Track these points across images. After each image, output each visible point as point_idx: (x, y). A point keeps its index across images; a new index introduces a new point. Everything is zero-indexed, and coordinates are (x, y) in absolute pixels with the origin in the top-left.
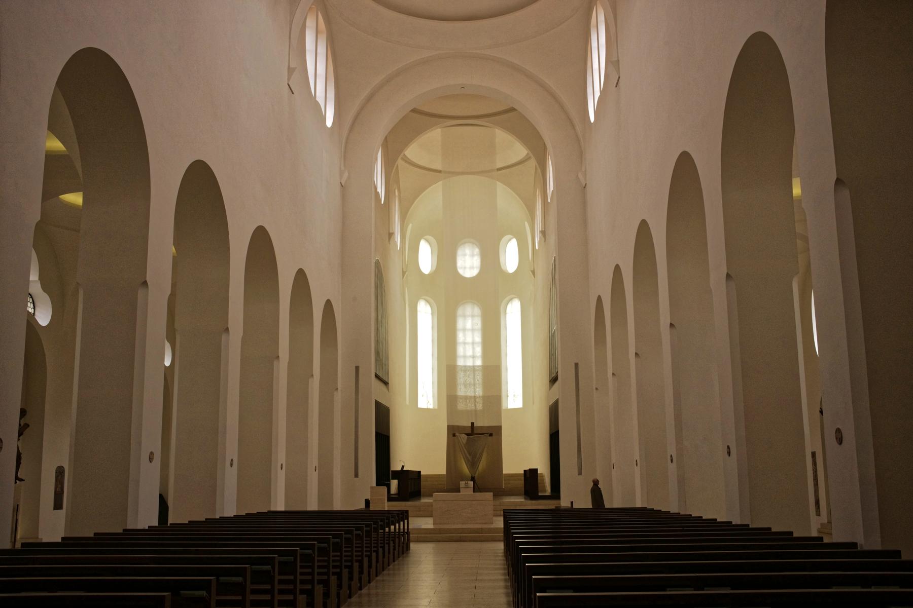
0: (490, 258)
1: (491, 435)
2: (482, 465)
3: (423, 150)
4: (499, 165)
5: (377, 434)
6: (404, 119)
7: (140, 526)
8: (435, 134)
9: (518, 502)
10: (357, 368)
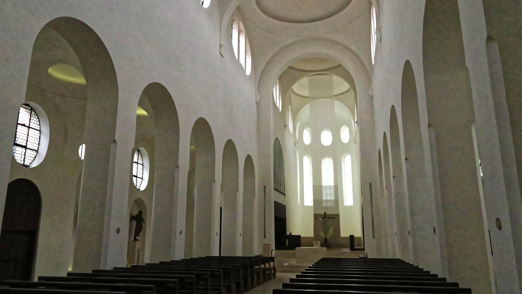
0: (336, 136)
1: (334, 218)
2: (331, 231)
3: (301, 86)
4: (336, 93)
7: (109, 267)
8: (305, 80)
9: (346, 253)
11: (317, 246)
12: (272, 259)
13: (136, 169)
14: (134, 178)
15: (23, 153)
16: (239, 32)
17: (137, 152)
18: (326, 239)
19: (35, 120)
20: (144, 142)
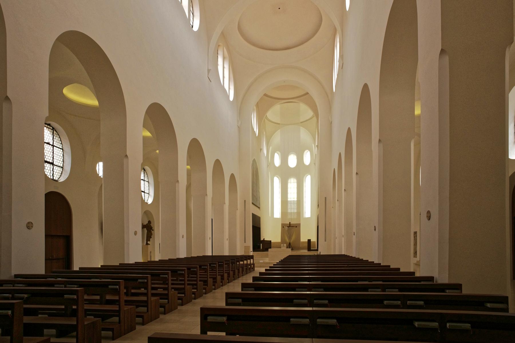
0: (300, 159)
2: (293, 238)
3: (274, 114)
4: (302, 120)
5: (253, 226)
6: (262, 99)
7: (132, 261)
8: (277, 108)
9: (305, 252)
10: (245, 201)
11: (284, 247)
12: (252, 257)
13: (144, 186)
14: (143, 193)
15: (52, 170)
16: (224, 58)
17: (143, 171)
18: (290, 243)
19: (57, 139)
20: (149, 162)
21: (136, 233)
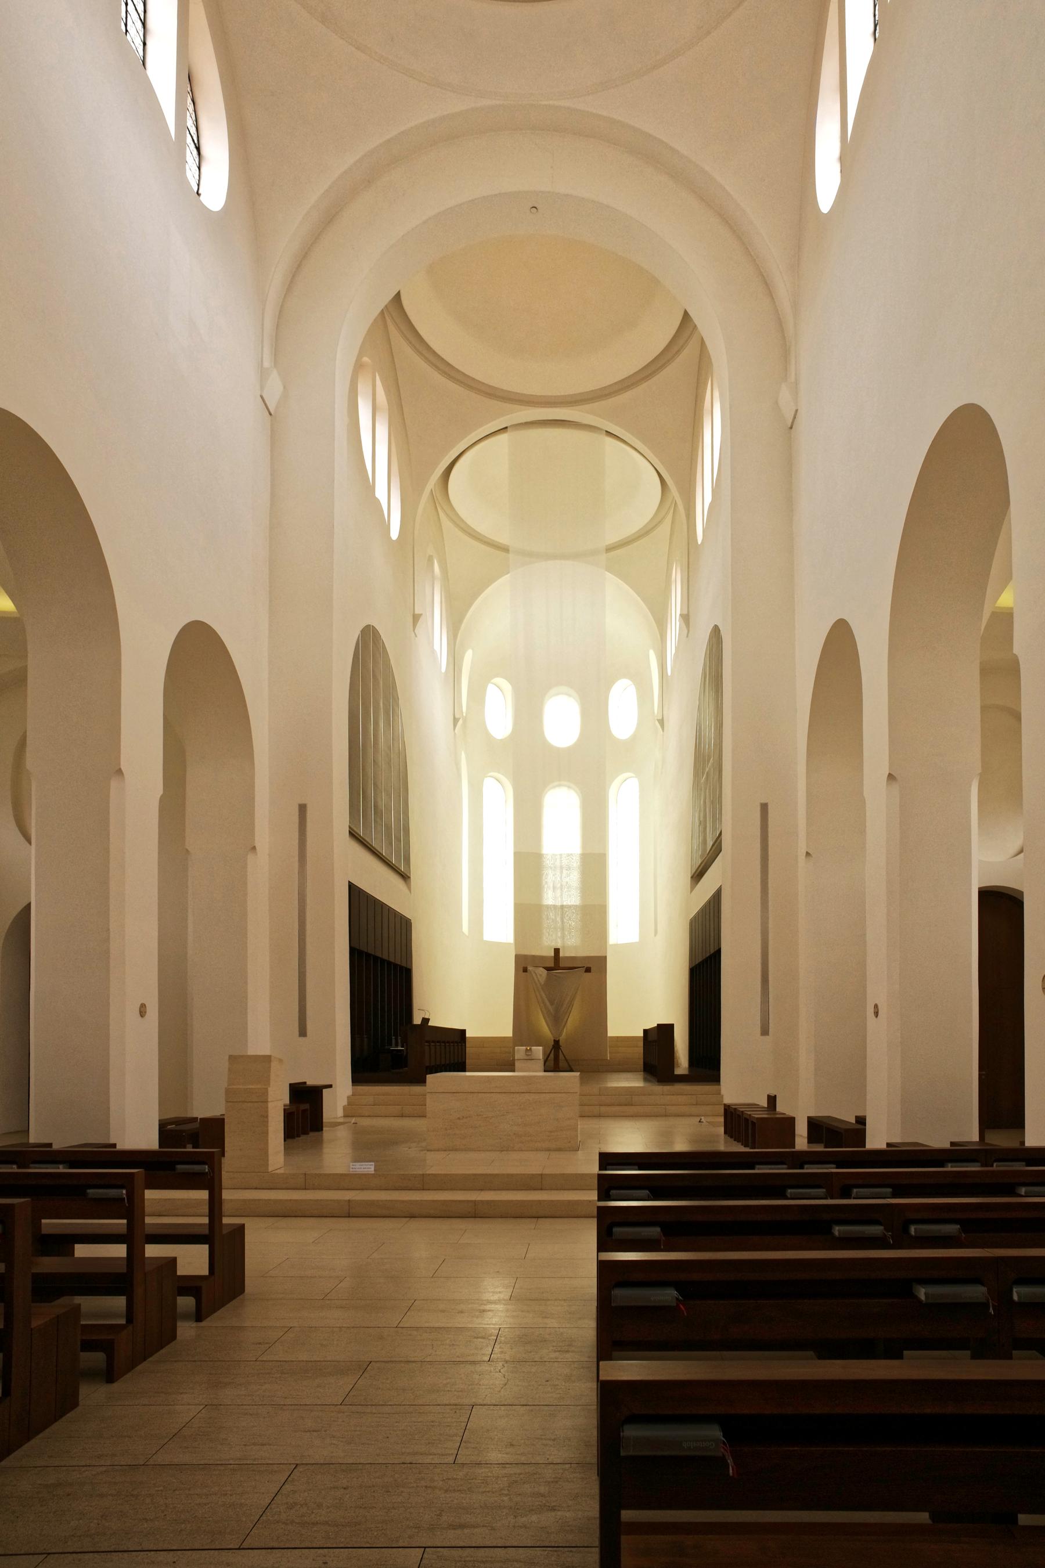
0: (594, 712)
1: (588, 970)
2: (573, 1020)
3: (485, 477)
4: (612, 538)
10: (303, 809)
11: (531, 1069)
18: (557, 1044)
21: (143, 1011)
